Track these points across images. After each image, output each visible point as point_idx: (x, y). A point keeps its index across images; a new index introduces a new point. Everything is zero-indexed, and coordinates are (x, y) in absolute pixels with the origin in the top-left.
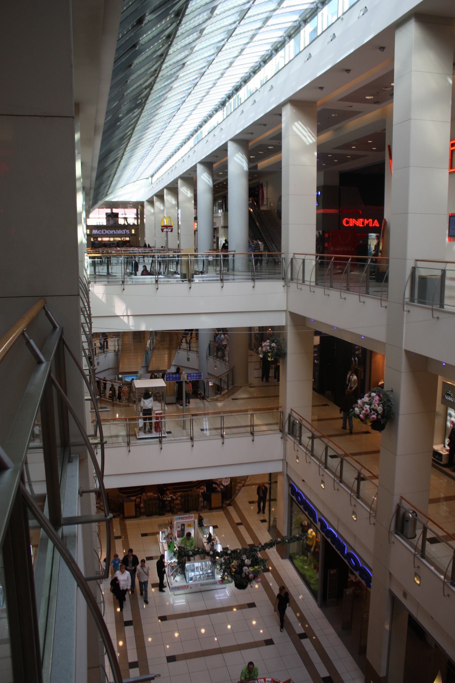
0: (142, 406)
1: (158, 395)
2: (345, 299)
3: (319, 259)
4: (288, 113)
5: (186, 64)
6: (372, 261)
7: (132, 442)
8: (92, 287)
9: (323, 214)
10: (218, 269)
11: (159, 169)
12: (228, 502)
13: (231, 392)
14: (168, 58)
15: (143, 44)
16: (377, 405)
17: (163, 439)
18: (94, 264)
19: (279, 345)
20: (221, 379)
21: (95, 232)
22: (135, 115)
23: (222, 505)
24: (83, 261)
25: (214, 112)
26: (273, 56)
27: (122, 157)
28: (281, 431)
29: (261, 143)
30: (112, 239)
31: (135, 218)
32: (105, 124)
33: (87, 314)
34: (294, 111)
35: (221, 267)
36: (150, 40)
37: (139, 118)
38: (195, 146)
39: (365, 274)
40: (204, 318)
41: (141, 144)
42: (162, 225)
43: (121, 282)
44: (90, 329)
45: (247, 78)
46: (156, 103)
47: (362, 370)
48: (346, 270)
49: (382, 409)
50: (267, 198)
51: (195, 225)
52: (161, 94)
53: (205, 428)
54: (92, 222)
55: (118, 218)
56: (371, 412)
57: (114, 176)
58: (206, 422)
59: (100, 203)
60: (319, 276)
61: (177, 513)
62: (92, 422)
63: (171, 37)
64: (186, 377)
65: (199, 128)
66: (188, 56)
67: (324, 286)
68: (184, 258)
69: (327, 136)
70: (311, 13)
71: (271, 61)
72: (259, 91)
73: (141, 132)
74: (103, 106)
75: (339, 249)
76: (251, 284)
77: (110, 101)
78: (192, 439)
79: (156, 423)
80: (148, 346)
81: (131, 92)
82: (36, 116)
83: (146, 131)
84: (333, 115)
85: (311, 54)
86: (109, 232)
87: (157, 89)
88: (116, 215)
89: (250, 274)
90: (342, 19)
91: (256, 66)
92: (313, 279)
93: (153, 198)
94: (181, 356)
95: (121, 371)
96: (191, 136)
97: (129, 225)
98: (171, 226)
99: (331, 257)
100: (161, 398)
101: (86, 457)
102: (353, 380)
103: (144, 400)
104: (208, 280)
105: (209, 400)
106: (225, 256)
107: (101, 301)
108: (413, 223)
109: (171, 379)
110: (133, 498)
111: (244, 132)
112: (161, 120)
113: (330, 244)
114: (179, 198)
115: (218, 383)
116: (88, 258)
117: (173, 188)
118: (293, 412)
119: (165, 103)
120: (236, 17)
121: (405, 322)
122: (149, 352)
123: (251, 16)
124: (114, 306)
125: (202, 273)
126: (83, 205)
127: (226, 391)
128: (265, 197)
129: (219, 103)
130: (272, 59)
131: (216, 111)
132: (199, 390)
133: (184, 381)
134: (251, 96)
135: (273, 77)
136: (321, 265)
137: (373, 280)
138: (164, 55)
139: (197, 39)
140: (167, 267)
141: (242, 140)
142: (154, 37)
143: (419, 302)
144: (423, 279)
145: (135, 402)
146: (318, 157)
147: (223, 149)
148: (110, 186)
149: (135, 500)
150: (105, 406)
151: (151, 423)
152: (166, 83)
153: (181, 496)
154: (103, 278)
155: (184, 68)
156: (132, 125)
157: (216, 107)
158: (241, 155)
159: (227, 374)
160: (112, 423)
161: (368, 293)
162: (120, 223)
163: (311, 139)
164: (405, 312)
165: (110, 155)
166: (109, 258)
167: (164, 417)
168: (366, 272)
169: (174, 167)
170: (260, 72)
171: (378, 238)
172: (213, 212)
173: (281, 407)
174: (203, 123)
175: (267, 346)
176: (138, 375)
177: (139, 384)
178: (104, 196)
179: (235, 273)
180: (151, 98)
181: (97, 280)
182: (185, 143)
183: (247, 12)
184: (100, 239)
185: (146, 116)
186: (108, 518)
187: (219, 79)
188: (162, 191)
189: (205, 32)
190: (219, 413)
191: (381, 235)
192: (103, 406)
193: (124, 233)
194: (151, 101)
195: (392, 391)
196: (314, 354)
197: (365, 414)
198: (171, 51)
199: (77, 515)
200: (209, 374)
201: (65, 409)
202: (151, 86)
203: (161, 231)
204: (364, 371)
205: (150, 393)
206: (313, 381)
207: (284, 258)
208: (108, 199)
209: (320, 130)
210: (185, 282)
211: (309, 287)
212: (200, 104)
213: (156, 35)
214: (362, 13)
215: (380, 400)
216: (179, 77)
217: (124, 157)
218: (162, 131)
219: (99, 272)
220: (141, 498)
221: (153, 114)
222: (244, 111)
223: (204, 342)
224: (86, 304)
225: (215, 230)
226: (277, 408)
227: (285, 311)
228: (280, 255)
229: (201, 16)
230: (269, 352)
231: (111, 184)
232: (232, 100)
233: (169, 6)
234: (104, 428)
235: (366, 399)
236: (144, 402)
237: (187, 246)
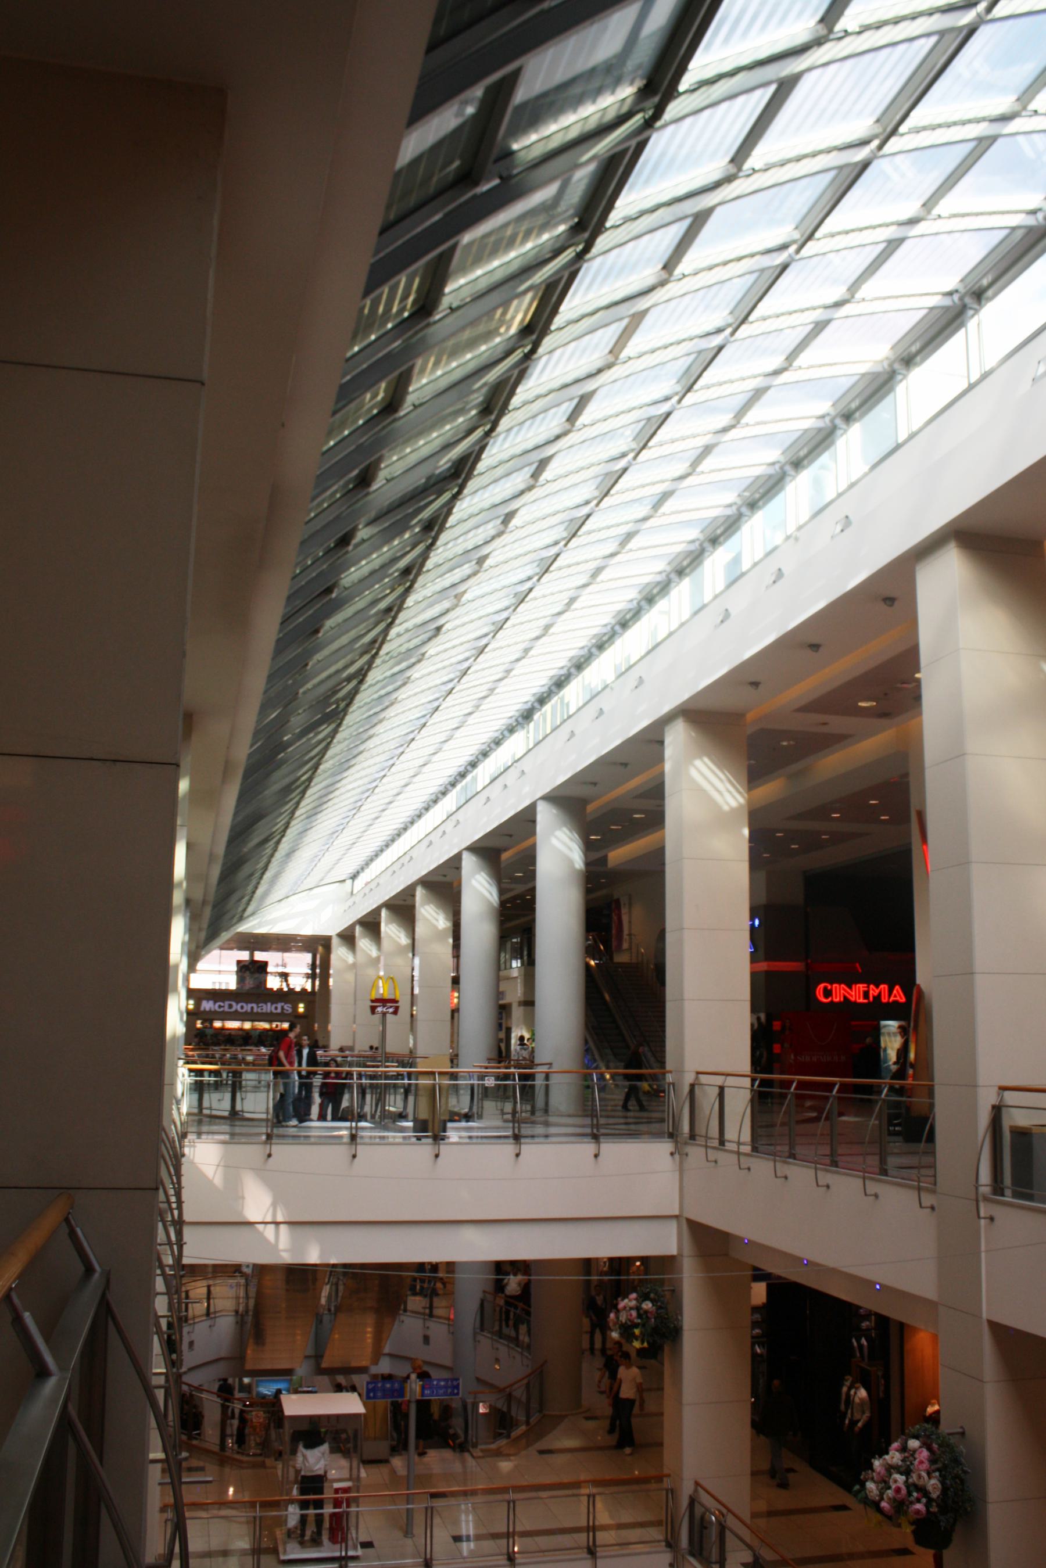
1: (344, 1436)
2: (828, 1187)
3: (759, 1086)
4: (678, 739)
5: (444, 629)
6: (892, 1089)
8: (190, 1146)
9: (767, 972)
10: (508, 1107)
11: (372, 860)
13: (537, 1432)
14: (402, 616)
15: (347, 585)
16: (924, 1474)
18: (199, 1088)
19: (660, 1308)
20: (510, 1395)
21: (207, 1005)
22: (320, 736)
24: (174, 1074)
25: (506, 733)
26: (643, 612)
27: (284, 831)
28: (669, 1545)
29: (618, 807)
30: (247, 1025)
31: (308, 976)
32: (250, 756)
33: (174, 1188)
34: (693, 734)
35: (515, 1103)
36: (361, 581)
37: (329, 744)
38: (458, 809)
39: (877, 1122)
40: (469, 1234)
41: (330, 804)
42: (373, 997)
43: (264, 1137)
45: (582, 660)
46: (371, 712)
47: (880, 1373)
48: (828, 1113)
49: (940, 1486)
50: (630, 935)
51: (453, 997)
52: (383, 692)
53: (464, 1533)
54: (201, 981)
55: (267, 973)
56: (909, 1494)
57: (263, 874)
58: (467, 1515)
59: (225, 936)
60: (761, 1127)
62: (163, 1509)
63: (410, 574)
64: (418, 1389)
65: (469, 768)
66: (447, 611)
67: (774, 1154)
68: (423, 1082)
69: (771, 789)
70: (726, 525)
71: (638, 624)
72: (612, 688)
73: (333, 775)
74: (248, 719)
75: (808, 1059)
76: (588, 1148)
77: (265, 707)
79: (333, 1515)
80: (323, 1301)
81: (315, 687)
82: (92, 759)
83: (345, 774)
84: (785, 743)
85: (730, 610)
86: (242, 1007)
87: (374, 682)
88: (262, 967)
89: (588, 1121)
90: (797, 539)
91: (605, 634)
92: (746, 1136)
93: (354, 929)
94: (407, 1327)
95: (249, 1366)
96: (449, 787)
97: (291, 991)
98: (394, 1001)
99: (791, 1082)
100: (350, 1445)
102: (857, 1400)
103: (304, 1451)
104: (482, 1137)
105: (477, 1452)
106: (524, 1077)
107: (209, 1182)
108: (988, 995)
109: (379, 1394)
111: (577, 779)
112: (380, 749)
113: (786, 1045)
114: (417, 929)
115: (501, 1404)
116: (186, 1072)
117: (402, 908)
118: (701, 1491)
119: (391, 712)
120: (560, 533)
121: (983, 1248)
122: (326, 1318)
123: (594, 531)
124: (243, 1198)
125: (468, 1117)
126: (183, 944)
127: (524, 1428)
128: (626, 931)
129: (517, 714)
130: (639, 619)
131: (511, 730)
133: (413, 1399)
134: (592, 698)
135: (642, 658)
136: (763, 1098)
137: (896, 1138)
138: (395, 609)
139: (469, 577)
140: (380, 1101)
141: (571, 800)
142: (372, 573)
143: (1016, 1195)
144: (1022, 1135)
145: (280, 1454)
146: (751, 839)
147: (525, 820)
148: (252, 897)
150: (201, 1464)
151: (319, 1519)
152: (396, 669)
154: (219, 1124)
155: (439, 637)
156: (312, 758)
157: (510, 721)
158: (567, 832)
159: (525, 1381)
160: (215, 1512)
161: (884, 1172)
162: (269, 985)
163: (733, 796)
164: (983, 1222)
165: (255, 827)
166: (237, 1074)
167: (356, 1500)
168: (879, 1117)
169: (407, 858)
170: (613, 647)
171: (904, 1031)
172: (499, 967)
173: (669, 1476)
174: (480, 757)
175: (631, 1308)
176: (294, 1378)
177: (295, 1406)
178: (235, 920)
179: (552, 1119)
180: (361, 699)
181: (205, 1128)
182: (435, 802)
183: (583, 523)
184: (217, 1024)
185: (345, 739)
187: (518, 660)
188: (376, 912)
189: (488, 562)
190: (504, 1490)
191: (912, 1024)
192: (195, 1463)
193: (279, 1011)
194: (360, 707)
195: (963, 1434)
196: (753, 1329)
197: (895, 1499)
198: (410, 601)
200: (478, 1379)
201: (93, 1498)
202: (361, 675)
203: (369, 1011)
204: (887, 1376)
205: (323, 1430)
206: (753, 1404)
207: (673, 1084)
208: (244, 927)
209: (754, 777)
210: (424, 1140)
211: (735, 1157)
212: (473, 716)
213: (377, 567)
214: (839, 528)
215: (933, 1461)
216: (427, 655)
217: (289, 831)
218: (383, 773)
219: (210, 1108)
221: (363, 737)
222: (576, 732)
223: (470, 1294)
224: (173, 1199)
225: (503, 1010)
226: (659, 1479)
227: (676, 1217)
228: (664, 1074)
229: (481, 530)
230: (636, 1326)
231: (254, 892)
232: (548, 708)
233: (410, 510)
234: (193, 1530)
235: (894, 1457)
236: (304, 1456)
237: (429, 1044)
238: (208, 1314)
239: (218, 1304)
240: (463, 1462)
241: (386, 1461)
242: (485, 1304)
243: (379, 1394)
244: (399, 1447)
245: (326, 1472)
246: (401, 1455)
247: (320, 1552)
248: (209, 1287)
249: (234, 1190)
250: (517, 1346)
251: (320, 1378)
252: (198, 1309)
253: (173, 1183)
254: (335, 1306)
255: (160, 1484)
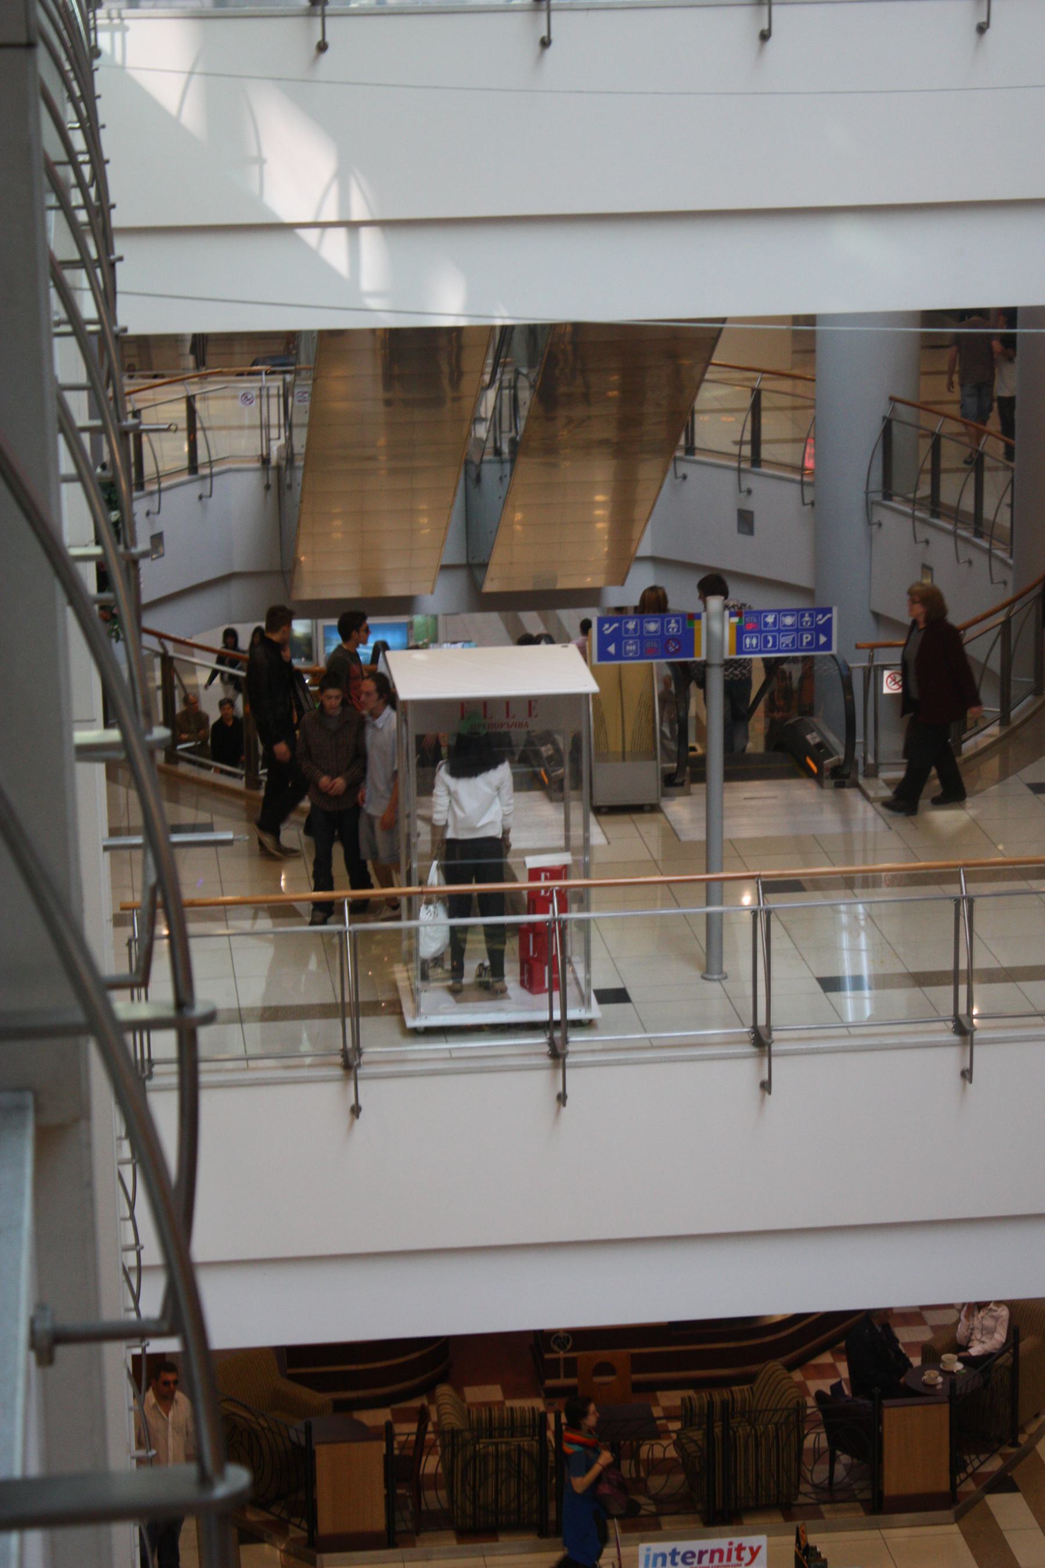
0: (439, 818)
7: (371, 1051)
8: (112, 29)
12: (994, 1465)
17: (576, 1039)
23: (953, 1485)
33: (87, 205)
40: (851, 239)
44: (107, 297)
53: (847, 971)
58: (854, 933)
61: (658, 1526)
62: (119, 921)
78: (761, 1040)
101: (83, 1113)
107: (175, 121)
109: (631, 648)
110: (376, 1418)
122: (490, 472)
124: (261, 161)
127: (994, 730)
132: (817, 720)
133: (716, 660)
149: (388, 1433)
150: (203, 817)
153: (686, 1414)
159: (1000, 617)
160: (246, 925)
176: (418, 619)
177: (423, 675)
186: (221, 1491)
199: (17, 1472)
200: (877, 616)
220: (422, 1416)
223: (858, 398)
224: (79, 141)
238: (193, 467)
239: (216, 445)
240: (845, 814)
241: (654, 808)
242: (896, 428)
243: (631, 648)
244: (683, 772)
245: (506, 832)
246: (688, 793)
247: (501, 1010)
248: (190, 400)
249: (232, 139)
250: (979, 534)
251: (479, 617)
252: (166, 452)
253: (72, 97)
254: (513, 442)
255: (106, 848)
